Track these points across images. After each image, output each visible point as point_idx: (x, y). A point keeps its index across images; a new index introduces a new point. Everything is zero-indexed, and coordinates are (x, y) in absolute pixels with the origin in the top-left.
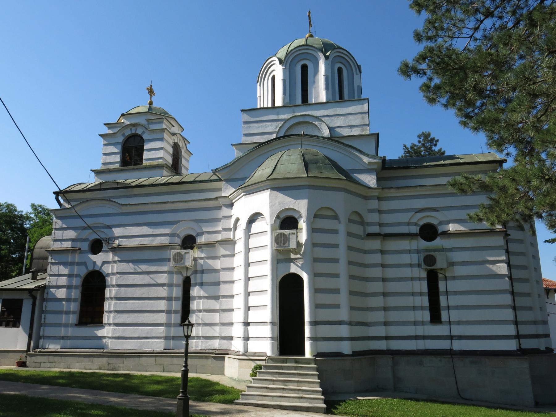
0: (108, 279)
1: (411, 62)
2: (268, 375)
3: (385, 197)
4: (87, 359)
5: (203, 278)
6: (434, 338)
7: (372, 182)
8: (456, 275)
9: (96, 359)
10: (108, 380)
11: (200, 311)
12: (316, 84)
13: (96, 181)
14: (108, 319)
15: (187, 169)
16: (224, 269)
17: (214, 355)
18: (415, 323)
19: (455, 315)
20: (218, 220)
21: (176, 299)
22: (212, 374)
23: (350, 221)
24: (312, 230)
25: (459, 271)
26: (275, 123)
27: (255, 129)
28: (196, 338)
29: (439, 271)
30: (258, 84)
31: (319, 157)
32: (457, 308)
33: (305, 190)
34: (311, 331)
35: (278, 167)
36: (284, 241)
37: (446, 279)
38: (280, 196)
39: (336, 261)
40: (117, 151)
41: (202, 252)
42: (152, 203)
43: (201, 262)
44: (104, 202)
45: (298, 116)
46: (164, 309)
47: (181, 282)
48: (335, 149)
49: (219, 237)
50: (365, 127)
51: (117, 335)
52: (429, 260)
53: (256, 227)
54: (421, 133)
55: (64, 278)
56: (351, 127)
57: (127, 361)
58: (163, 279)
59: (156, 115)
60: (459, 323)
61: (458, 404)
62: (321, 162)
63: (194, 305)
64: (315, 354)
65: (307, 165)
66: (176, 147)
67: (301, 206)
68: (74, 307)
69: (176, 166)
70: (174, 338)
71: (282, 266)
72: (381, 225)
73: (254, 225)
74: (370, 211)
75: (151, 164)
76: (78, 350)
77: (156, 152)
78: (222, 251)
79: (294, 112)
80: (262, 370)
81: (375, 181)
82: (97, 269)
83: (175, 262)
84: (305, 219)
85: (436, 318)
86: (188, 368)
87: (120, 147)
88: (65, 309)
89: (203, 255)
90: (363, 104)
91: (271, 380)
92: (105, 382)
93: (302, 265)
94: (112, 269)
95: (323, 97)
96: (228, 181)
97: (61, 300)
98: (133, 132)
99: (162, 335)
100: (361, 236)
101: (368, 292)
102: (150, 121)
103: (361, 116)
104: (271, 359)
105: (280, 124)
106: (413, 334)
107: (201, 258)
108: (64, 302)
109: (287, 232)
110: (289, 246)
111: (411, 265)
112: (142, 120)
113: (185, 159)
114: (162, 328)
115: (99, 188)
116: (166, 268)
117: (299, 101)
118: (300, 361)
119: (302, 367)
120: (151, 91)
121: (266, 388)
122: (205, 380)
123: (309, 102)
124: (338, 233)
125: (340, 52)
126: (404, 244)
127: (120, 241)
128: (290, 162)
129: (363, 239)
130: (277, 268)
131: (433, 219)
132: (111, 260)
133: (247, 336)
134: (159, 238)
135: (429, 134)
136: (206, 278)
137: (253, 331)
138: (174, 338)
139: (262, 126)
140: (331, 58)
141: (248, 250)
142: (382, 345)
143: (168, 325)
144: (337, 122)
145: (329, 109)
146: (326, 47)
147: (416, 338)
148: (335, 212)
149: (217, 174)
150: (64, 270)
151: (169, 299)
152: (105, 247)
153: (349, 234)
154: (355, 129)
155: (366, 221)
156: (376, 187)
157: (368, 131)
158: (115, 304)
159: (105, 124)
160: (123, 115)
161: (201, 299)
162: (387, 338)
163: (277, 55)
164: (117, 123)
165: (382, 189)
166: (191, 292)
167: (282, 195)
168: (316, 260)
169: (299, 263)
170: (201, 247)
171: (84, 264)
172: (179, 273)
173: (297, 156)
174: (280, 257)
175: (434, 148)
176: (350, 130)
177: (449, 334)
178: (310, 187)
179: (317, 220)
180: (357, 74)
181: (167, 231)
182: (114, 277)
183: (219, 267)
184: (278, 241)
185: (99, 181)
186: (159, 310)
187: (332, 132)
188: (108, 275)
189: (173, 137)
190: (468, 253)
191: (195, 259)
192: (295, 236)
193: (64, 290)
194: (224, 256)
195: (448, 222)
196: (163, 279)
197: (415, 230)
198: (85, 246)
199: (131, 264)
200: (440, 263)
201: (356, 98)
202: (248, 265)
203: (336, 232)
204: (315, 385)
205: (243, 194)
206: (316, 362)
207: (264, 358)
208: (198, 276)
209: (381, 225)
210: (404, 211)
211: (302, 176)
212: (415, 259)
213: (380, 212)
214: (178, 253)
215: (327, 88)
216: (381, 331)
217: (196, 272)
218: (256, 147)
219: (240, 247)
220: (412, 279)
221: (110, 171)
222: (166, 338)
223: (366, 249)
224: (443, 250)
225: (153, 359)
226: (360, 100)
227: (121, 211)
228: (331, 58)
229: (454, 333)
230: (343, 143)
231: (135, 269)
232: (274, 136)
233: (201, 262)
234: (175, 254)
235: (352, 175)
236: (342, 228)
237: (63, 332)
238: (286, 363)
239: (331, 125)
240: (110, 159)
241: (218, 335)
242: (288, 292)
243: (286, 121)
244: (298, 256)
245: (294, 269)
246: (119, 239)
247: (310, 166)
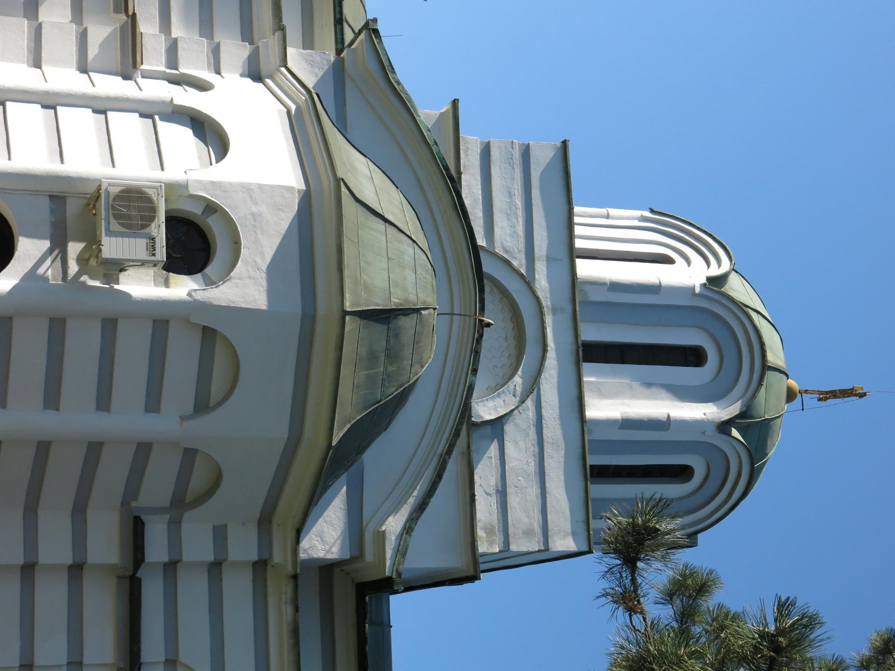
1: (710, 602)
7: (319, 546)
12: (642, 389)
20: (206, 27)
23: (190, 455)
24: (161, 319)
26: (522, 246)
30: (647, 214)
33: (298, 301)
36: (129, 217)
38: (282, 220)
45: (543, 322)
48: (433, 424)
49: (148, 27)
50: (499, 538)
53: (179, 139)
56: (502, 493)
62: (391, 369)
65: (381, 317)
67: (243, 286)
72: (171, 567)
74: (220, 534)
78: (100, 32)
79: (554, 311)
81: (321, 555)
84: (199, 296)
90: (574, 534)
93: (44, 278)
95: (599, 409)
96: (338, 71)
100: (136, 498)
103: (537, 527)
105: (519, 262)
109: (159, 230)
110: (110, 233)
117: (591, 333)
123: (586, 366)
125: (739, 475)
128: (392, 264)
129: (125, 504)
130: (36, 193)
139: (512, 204)
140: (720, 441)
141: (100, 106)
144: (518, 448)
146: (754, 430)
148: (219, 404)
153: (143, 451)
154: (495, 507)
155: (187, 515)
156: (302, 556)
163: (733, 275)
165: (295, 577)
167: (285, 225)
168: (57, 327)
169: (49, 270)
173: (412, 290)
174: (73, 208)
176: (492, 491)
178: (309, 320)
179: (197, 336)
183: (44, 15)
184: (129, 199)
187: (488, 430)
192: (143, 255)
194: (83, 38)
202: (50, 102)
203: (153, 404)
205: (293, 108)
209: (171, 567)
211: (347, 295)
213: (216, 568)
215: (628, 424)
218: (447, 168)
219: (110, 85)
223: (91, 514)
228: (720, 441)
230: (449, 452)
232: (481, 241)
235: (343, 478)
236: (167, 425)
239: (509, 428)
243: (528, 283)
245: (29, 250)
247: (379, 330)
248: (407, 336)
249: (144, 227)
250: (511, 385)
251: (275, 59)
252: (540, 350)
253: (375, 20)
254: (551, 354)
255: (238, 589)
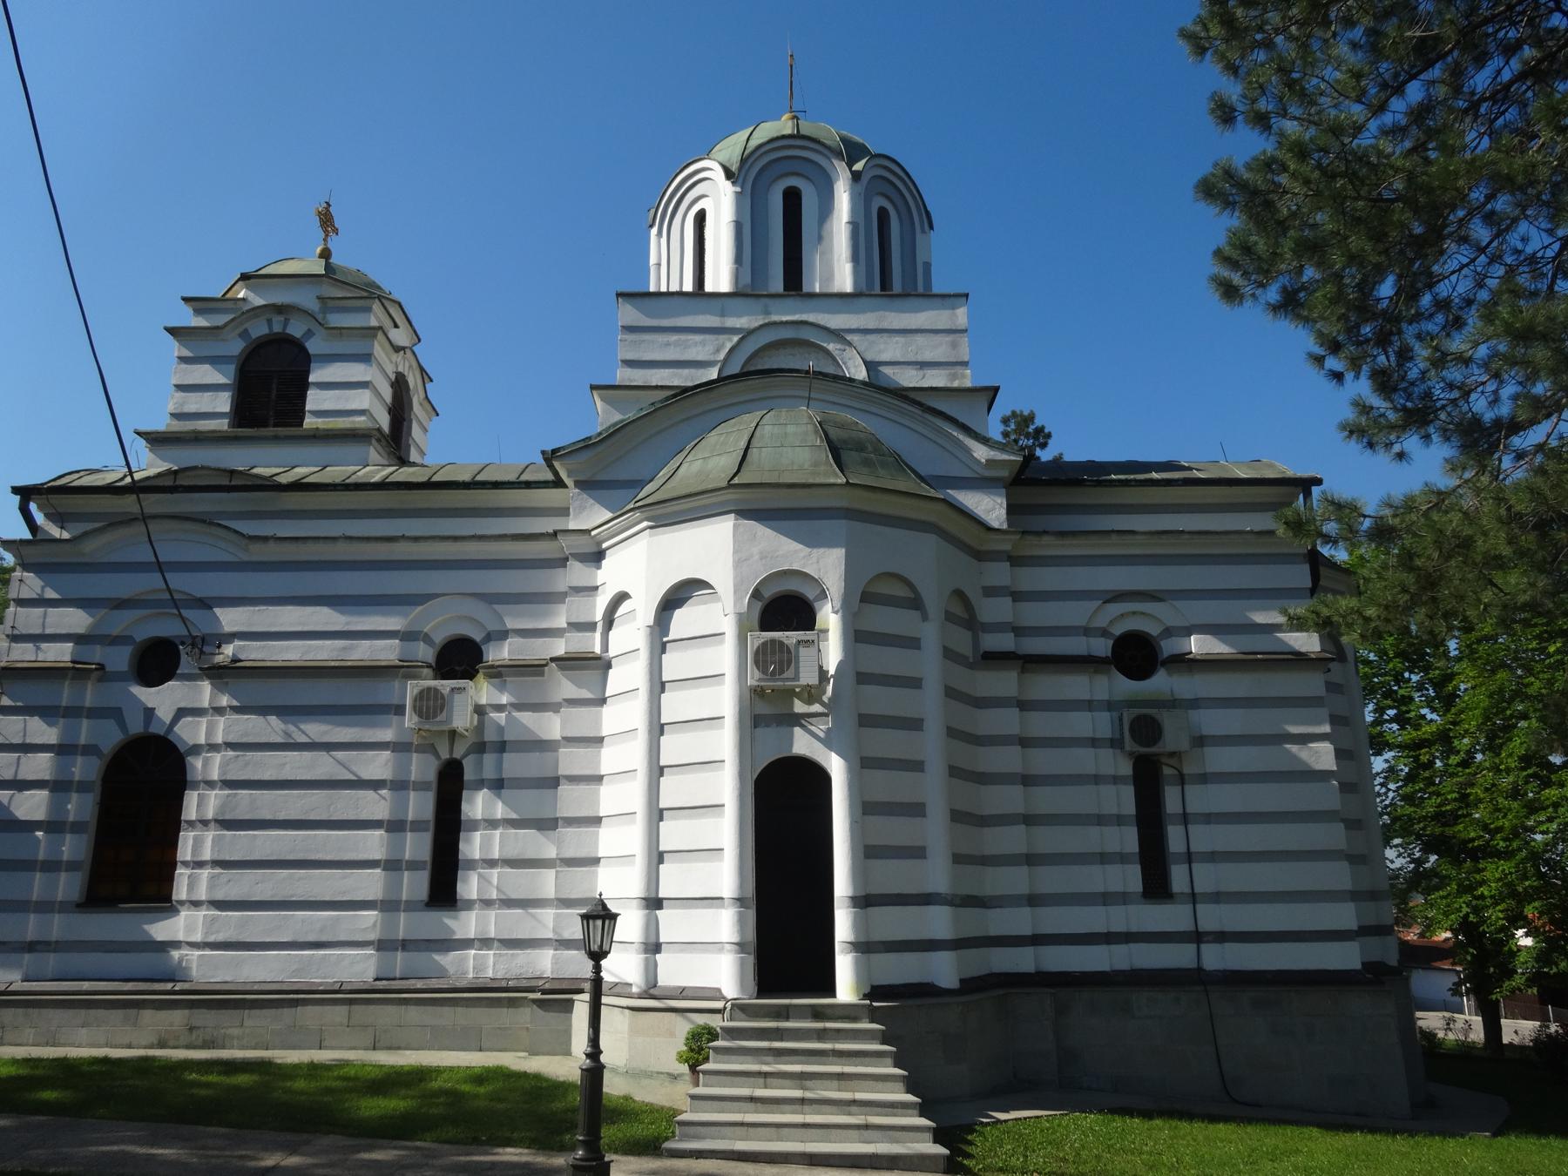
0: (196, 764)
2: (741, 1058)
3: (1032, 557)
4: (117, 1015)
5: (505, 765)
6: (1149, 937)
8: (1209, 769)
9: (147, 1015)
10: (207, 1085)
11: (491, 863)
13: (151, 465)
14: (192, 886)
15: (422, 453)
16: (570, 741)
17: (538, 996)
18: (1106, 899)
19: (1207, 877)
20: (551, 598)
21: (417, 826)
22: (534, 1053)
24: (856, 636)
25: (1219, 759)
27: (655, 348)
28: (496, 944)
29: (1164, 760)
30: (654, 231)
31: (862, 435)
32: (1213, 857)
34: (858, 925)
35: (753, 452)
37: (1182, 780)
38: (764, 535)
39: (914, 724)
40: (222, 380)
41: (502, 688)
42: (351, 538)
43: (500, 717)
44: (188, 525)
45: (782, 323)
46: (377, 856)
47: (431, 775)
49: (560, 648)
50: (959, 370)
51: (220, 937)
52: (1145, 728)
53: (684, 621)
54: (1009, 413)
55: (45, 757)
57: (256, 1021)
58: (378, 765)
59: (347, 290)
60: (1217, 897)
61: (1226, 1119)
63: (473, 846)
64: (867, 990)
66: (399, 384)
67: (827, 567)
68: (73, 847)
69: (396, 441)
70: (405, 945)
71: (768, 734)
72: (1019, 631)
73: (678, 613)
74: (990, 592)
75: (330, 426)
76: (86, 986)
77: (342, 393)
78: (565, 687)
79: (767, 313)
80: (719, 1043)
81: (1004, 512)
82: (155, 729)
83: (420, 716)
84: (838, 605)
85: (1156, 887)
86: (603, 1058)
87: (232, 369)
88: (41, 856)
89: (504, 699)
91: (760, 1074)
92: (203, 1092)
93: (828, 731)
94: (209, 733)
95: (844, 278)
97: (31, 826)
98: (277, 328)
99: (372, 936)
100: (966, 658)
101: (986, 812)
102: (331, 303)
103: (949, 338)
104: (740, 1008)
106: (1099, 927)
107: (499, 708)
108: (39, 834)
110: (796, 678)
111: (1094, 742)
112: (305, 298)
113: (420, 423)
114: (371, 915)
115: (169, 482)
116: (387, 735)
117: (777, 285)
118: (829, 1011)
119: (838, 1030)
120: (326, 220)
121: (752, 1099)
122: (524, 1075)
123: (806, 289)
124: (919, 648)
125: (886, 168)
126: (1076, 685)
127: (240, 647)
128: (788, 441)
131: (1147, 620)
132: (206, 704)
133: (652, 940)
134: (366, 643)
135: (1030, 418)
136: (514, 765)
137: (671, 924)
138: (405, 945)
139: (676, 344)
140: (865, 179)
142: (1023, 960)
143: (388, 906)
144: (887, 350)
145: (863, 311)
147: (1109, 938)
149: (556, 464)
150: (43, 731)
151: (395, 826)
152: (187, 663)
156: (1005, 526)
157: (967, 380)
158: (216, 841)
159: (186, 300)
160: (245, 277)
161: (495, 828)
162: (1037, 940)
164: (223, 299)
166: (465, 807)
168: (866, 721)
169: (820, 728)
170: (498, 673)
171: (116, 714)
172: (429, 748)
174: (764, 709)
175: (1038, 452)
177: (1192, 928)
180: (923, 231)
181: (393, 622)
182: (217, 758)
185: (162, 467)
186: (364, 859)
188: (196, 750)
189: (394, 357)
190: (1238, 713)
191: (480, 710)
192: (812, 650)
193: (42, 795)
194: (573, 702)
195: (1188, 631)
196: (378, 765)
197: (1102, 647)
198: (120, 659)
199: (273, 719)
200: (1173, 737)
201: (921, 290)
203: (913, 643)
204: (890, 1085)
205: (645, 524)
206: (874, 1015)
207: (719, 1005)
208: (489, 759)
210: (1075, 598)
211: (832, 481)
212: (1101, 723)
213: (1017, 596)
214: (429, 689)
215: (855, 258)
216: (1018, 921)
217: (480, 748)
218: (667, 399)
219: (628, 676)
220: (1097, 779)
221: (197, 438)
222: (382, 945)
224: (1173, 704)
225: (343, 1009)
226: (929, 296)
227: (245, 558)
229: (1206, 925)
231: (287, 734)
232: (713, 374)
233: (500, 717)
234: (421, 692)
236: (931, 633)
237: (32, 927)
238: (787, 1018)
240: (195, 403)
241: (550, 935)
242: (784, 810)
243: (748, 334)
244: (817, 708)
245: (803, 744)
246: (238, 643)
248: (843, 434)
249: (789, 652)
250: (835, 353)
251: (583, 539)
252: (809, 328)
253: (543, 452)
254: (811, 318)
255: (1031, 578)
